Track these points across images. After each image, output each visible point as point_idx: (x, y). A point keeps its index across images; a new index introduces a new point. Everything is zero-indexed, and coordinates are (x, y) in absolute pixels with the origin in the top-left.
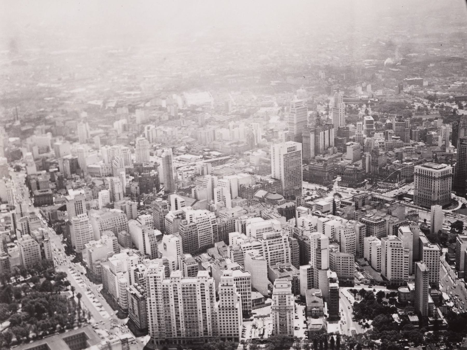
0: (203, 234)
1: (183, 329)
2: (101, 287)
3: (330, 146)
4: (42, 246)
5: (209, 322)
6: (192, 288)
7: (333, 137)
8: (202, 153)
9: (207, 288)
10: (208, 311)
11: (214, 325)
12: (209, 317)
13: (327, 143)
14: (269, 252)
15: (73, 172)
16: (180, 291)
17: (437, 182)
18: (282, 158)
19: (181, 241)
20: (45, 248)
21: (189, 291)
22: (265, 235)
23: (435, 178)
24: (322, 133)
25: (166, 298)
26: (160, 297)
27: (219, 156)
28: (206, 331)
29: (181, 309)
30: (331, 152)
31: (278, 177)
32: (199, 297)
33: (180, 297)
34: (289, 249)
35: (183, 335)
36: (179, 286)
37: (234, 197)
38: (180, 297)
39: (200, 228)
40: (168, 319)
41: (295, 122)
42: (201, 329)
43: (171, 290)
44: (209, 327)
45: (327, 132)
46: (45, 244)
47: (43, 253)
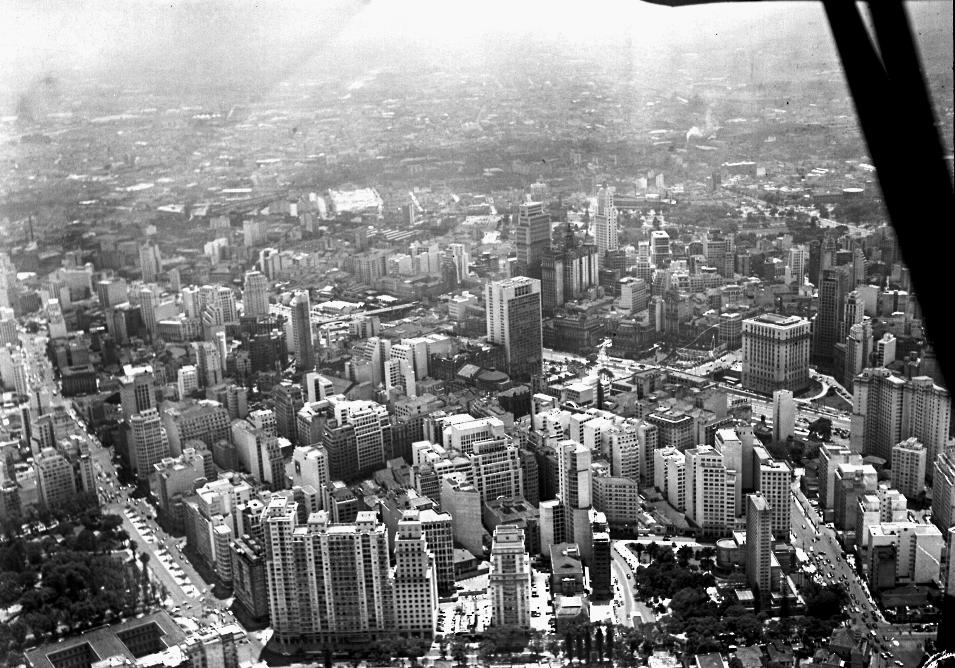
4: (77, 468)
8: (362, 299)
9: (373, 542)
10: (376, 584)
13: (585, 279)
14: (484, 476)
15: (131, 333)
16: (325, 549)
17: (783, 349)
22: (476, 445)
23: (779, 342)
24: (576, 262)
25: (301, 561)
26: (290, 559)
27: (393, 304)
28: (372, 621)
30: (594, 296)
32: (360, 558)
33: (326, 559)
34: (520, 470)
35: (332, 625)
37: (420, 376)
39: (360, 434)
41: (528, 242)
42: (365, 617)
43: (309, 546)
44: (379, 613)
45: (585, 259)
46: (82, 465)
47: (79, 479)
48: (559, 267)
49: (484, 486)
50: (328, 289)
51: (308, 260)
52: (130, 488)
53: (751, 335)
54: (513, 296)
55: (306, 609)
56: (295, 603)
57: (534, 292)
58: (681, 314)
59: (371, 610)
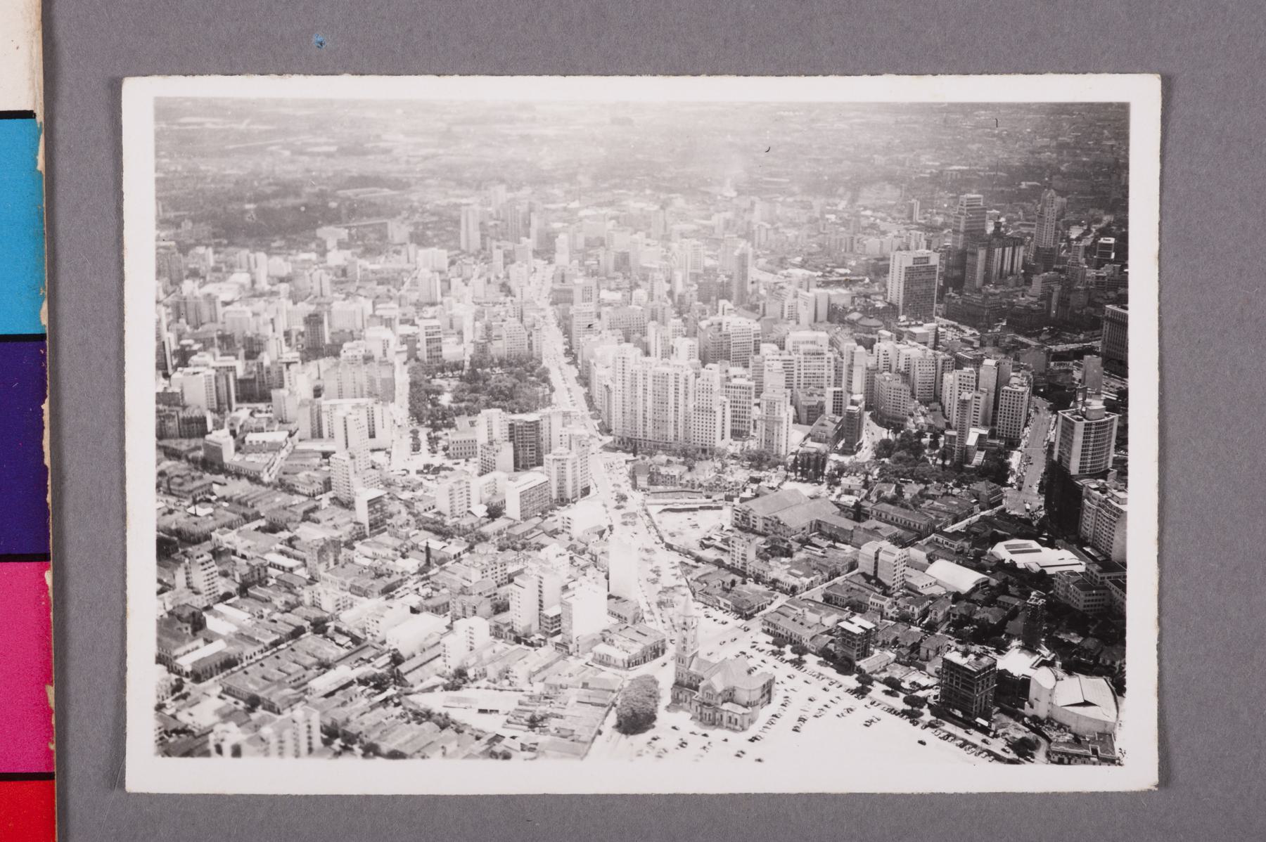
0: (737, 349)
1: (649, 429)
2: (586, 390)
3: (1011, 273)
4: (530, 335)
5: (680, 424)
6: (665, 377)
7: (1019, 261)
8: (821, 270)
9: (681, 380)
10: (681, 409)
11: (687, 429)
12: (681, 419)
13: (1007, 267)
14: (802, 371)
15: (617, 269)
16: (650, 380)
18: (903, 271)
19: (697, 347)
20: (534, 338)
21: (661, 379)
22: (802, 348)
25: (634, 386)
26: (628, 384)
29: (649, 404)
31: (894, 302)
32: (672, 390)
33: (650, 388)
34: (833, 372)
35: (650, 436)
36: (650, 374)
37: (819, 319)
38: (650, 388)
39: (733, 340)
40: (634, 413)
41: (962, 228)
42: (671, 433)
43: (640, 377)
44: (681, 434)
45: (1008, 250)
46: (534, 333)
47: (530, 345)
48: (982, 254)
49: (802, 379)
50: (799, 259)
51: (797, 237)
52: (569, 359)
53: (1111, 320)
54: (910, 264)
55: (634, 423)
56: (628, 417)
57: (932, 263)
58: (1073, 303)
59: (676, 429)
